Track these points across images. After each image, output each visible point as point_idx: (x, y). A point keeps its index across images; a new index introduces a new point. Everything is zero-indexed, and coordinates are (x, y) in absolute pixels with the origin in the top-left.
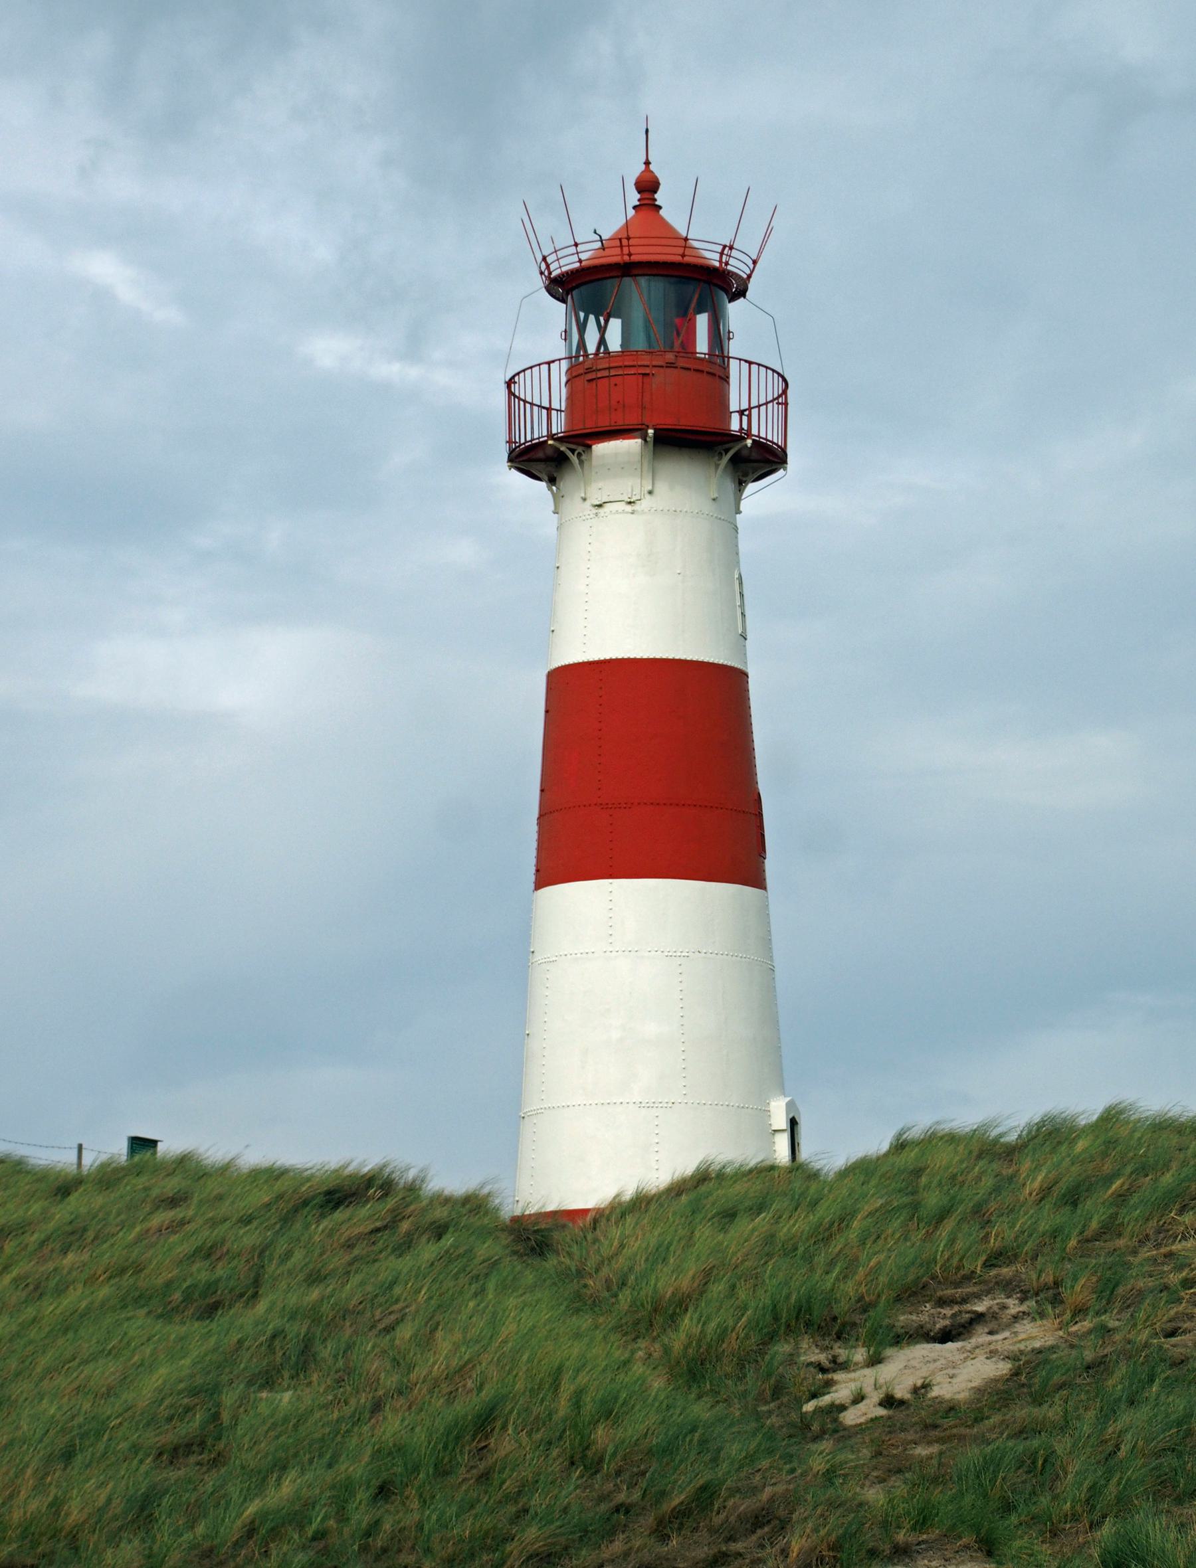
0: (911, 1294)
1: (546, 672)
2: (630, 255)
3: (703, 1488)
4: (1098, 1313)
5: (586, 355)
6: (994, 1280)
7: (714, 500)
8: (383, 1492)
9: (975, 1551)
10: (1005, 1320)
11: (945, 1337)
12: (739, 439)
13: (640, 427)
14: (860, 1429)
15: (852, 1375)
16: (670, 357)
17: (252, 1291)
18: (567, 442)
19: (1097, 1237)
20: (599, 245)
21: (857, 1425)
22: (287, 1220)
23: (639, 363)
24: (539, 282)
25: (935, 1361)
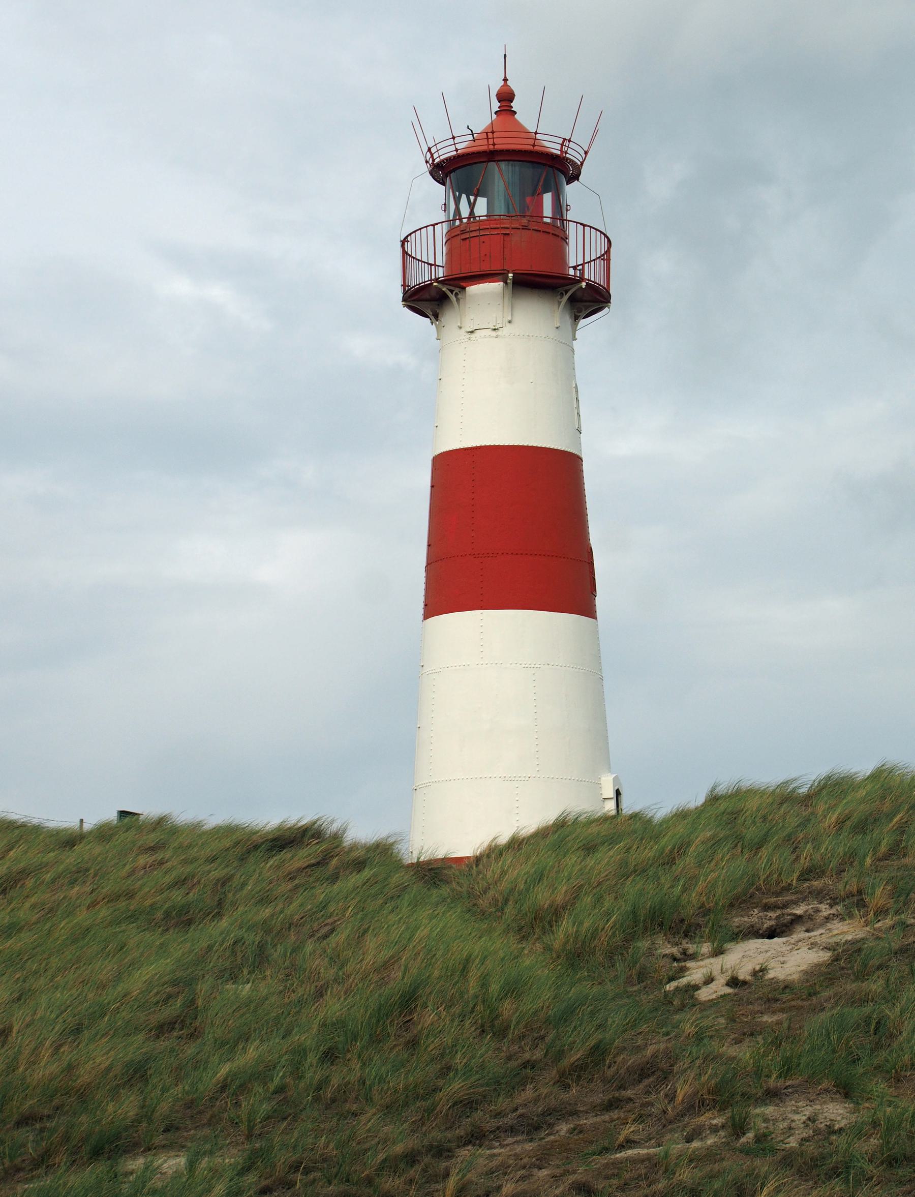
0: (739, 902)
1: (432, 457)
2: (494, 145)
3: (596, 1047)
4: (897, 913)
5: (461, 219)
6: (808, 890)
7: (557, 328)
8: (330, 1056)
9: (835, 1094)
10: (818, 921)
11: (771, 934)
12: (575, 281)
13: (502, 272)
14: (712, 1003)
15: (701, 963)
16: (524, 221)
17: (218, 911)
18: (447, 284)
19: (886, 857)
20: (471, 138)
21: (710, 1001)
22: (243, 859)
23: (502, 226)
24: (425, 168)
25: (766, 951)
